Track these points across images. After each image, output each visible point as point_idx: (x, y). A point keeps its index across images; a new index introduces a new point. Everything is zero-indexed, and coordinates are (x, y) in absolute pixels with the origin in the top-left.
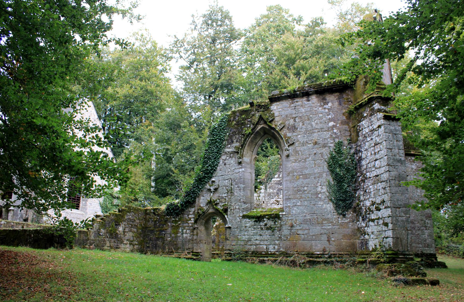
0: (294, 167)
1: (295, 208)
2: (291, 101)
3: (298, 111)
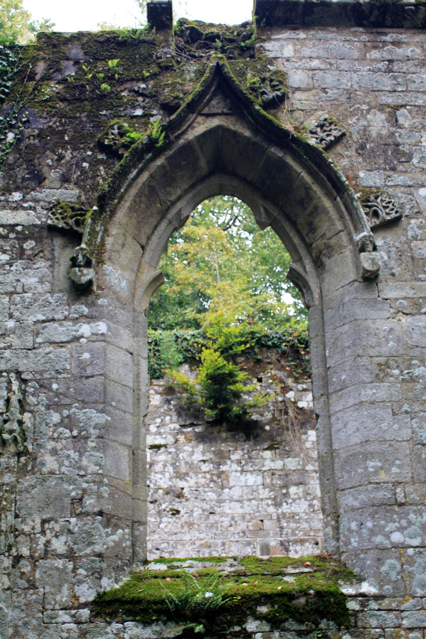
0: (408, 333)
2: (364, 38)
3: (407, 83)
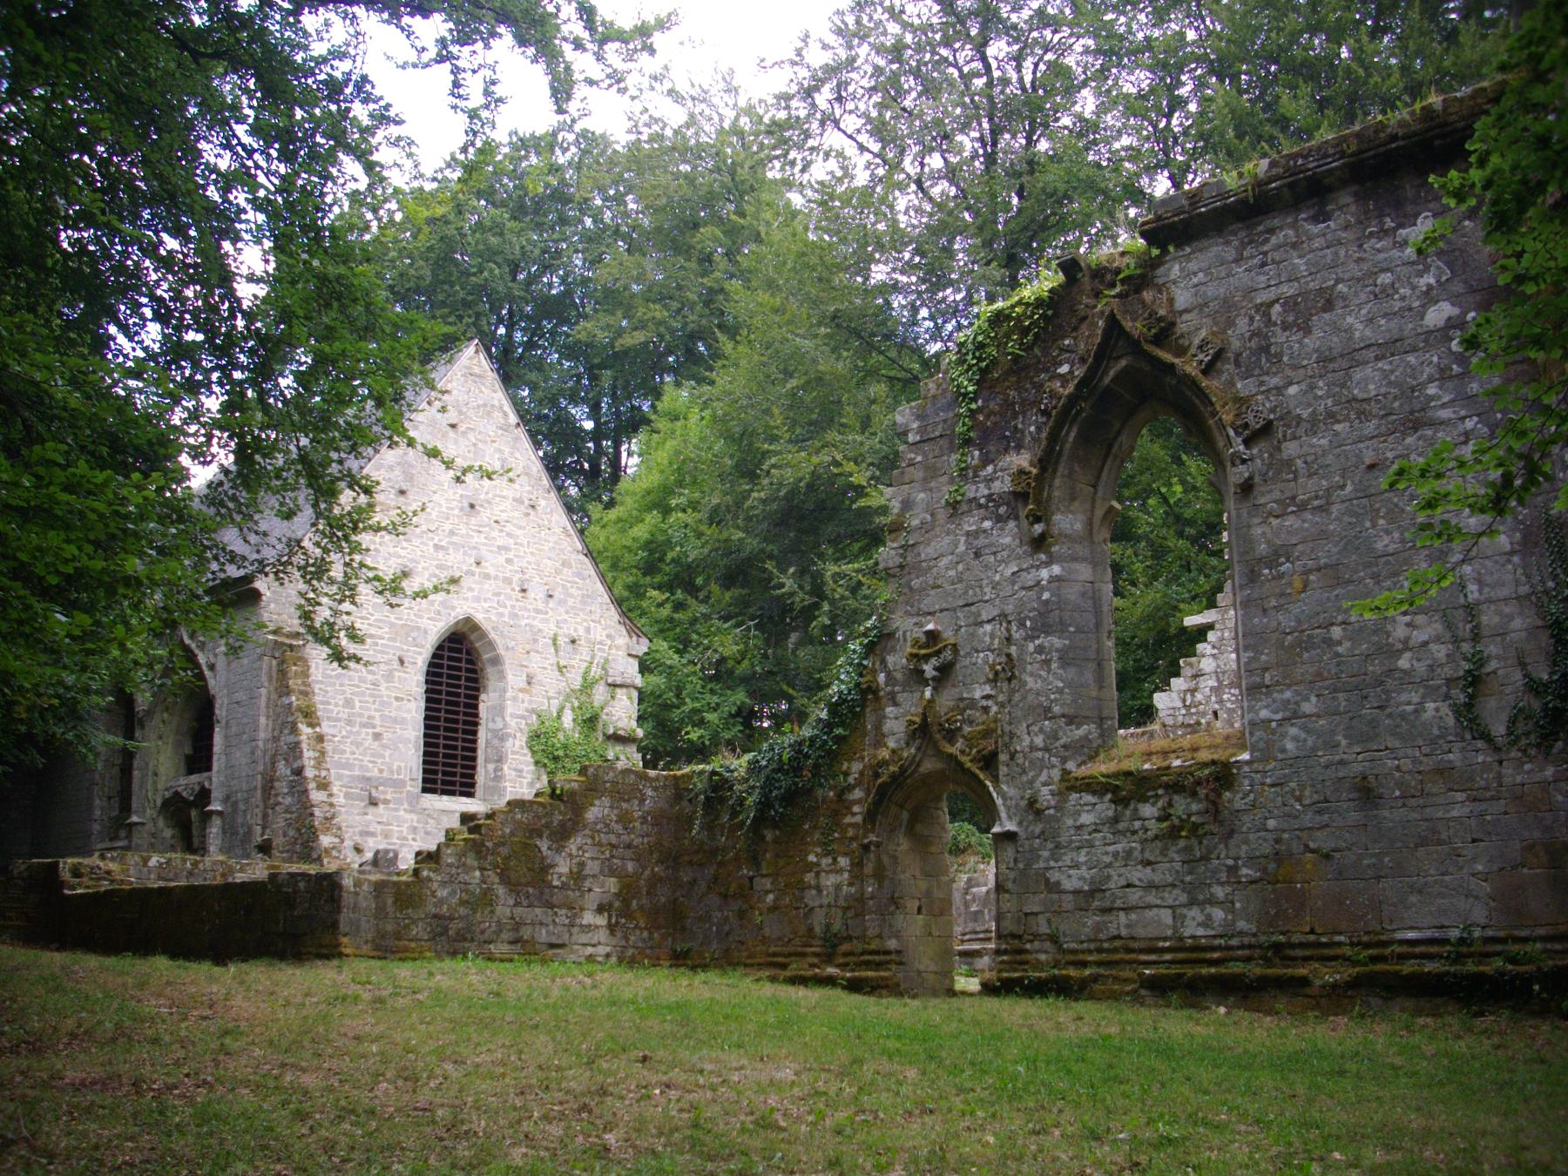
1: (1293, 731)
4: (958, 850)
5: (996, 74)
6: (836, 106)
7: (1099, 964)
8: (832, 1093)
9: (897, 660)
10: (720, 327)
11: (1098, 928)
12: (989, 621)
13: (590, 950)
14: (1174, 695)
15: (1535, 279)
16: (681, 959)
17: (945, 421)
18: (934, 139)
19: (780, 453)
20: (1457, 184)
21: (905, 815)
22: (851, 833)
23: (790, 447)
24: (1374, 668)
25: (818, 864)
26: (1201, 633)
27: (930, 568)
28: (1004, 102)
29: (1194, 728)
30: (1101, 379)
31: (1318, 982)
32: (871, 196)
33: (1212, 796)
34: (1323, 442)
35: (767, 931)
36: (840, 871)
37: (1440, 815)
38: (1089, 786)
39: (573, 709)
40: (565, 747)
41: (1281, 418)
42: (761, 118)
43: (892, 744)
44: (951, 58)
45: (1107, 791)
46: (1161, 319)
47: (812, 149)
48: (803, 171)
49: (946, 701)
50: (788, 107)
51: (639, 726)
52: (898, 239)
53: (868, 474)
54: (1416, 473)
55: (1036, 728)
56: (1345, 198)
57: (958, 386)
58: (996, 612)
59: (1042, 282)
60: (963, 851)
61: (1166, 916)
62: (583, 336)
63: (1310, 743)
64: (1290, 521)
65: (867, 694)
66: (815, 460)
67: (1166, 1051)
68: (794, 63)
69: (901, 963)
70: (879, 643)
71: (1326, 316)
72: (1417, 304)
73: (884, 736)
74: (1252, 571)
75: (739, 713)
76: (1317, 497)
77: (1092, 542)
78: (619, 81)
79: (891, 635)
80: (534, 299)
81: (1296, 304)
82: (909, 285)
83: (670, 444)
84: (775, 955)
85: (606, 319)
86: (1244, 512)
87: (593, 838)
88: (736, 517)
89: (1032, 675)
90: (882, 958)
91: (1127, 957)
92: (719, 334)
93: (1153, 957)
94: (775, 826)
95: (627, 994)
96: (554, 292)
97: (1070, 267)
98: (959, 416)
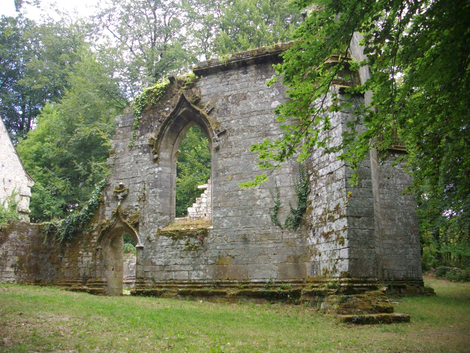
1: (226, 221)
2: (223, 75)
4: (127, 252)
5: (158, 19)
6: (108, 22)
7: (166, 287)
8: (80, 325)
9: (110, 193)
10: (66, 86)
11: (166, 276)
12: (139, 183)
13: (8, 279)
14: (194, 208)
15: (296, 96)
16: (38, 283)
17: (130, 121)
18: (137, 36)
19: (81, 127)
20: (280, 67)
21: (110, 240)
22: (93, 245)
23: (84, 125)
24: (250, 204)
25: (82, 254)
26: (203, 191)
27: (122, 166)
28: (159, 28)
29: (199, 218)
30: (178, 113)
31: (229, 294)
32: (116, 51)
33: (201, 238)
34: (240, 137)
35: (65, 275)
36: (89, 257)
37: (265, 247)
38: (165, 234)
39: (8, 203)
40: (5, 214)
41: (229, 130)
42: (84, 22)
43: (107, 218)
44: (145, 13)
45: (171, 236)
46: (197, 97)
47: (99, 34)
48: (96, 41)
49: (124, 206)
50: (93, 20)
51: (30, 209)
52: (123, 65)
53: (107, 136)
54: (259, 147)
55: (151, 216)
56: (252, 68)
57: (135, 111)
58: (141, 180)
59: (164, 82)
60: (129, 252)
61: (186, 273)
62: (21, 84)
63: (230, 224)
64: (229, 160)
65: (101, 202)
66: (91, 130)
67: (183, 313)
68: (96, 7)
69: (106, 286)
70: (105, 187)
71: (244, 101)
72: (269, 101)
73: (105, 216)
74: (217, 173)
75: (62, 206)
76: (237, 153)
77: (171, 162)
78: (37, 4)
79: (109, 185)
80: (6, 70)
81: (236, 97)
82: (125, 79)
83: (46, 121)
84: (68, 282)
85: (28, 79)
86: (216, 156)
87: (11, 244)
88: (65, 145)
89: (151, 200)
90: (101, 284)
91: (175, 285)
92: (65, 88)
93: (182, 285)
94: (70, 242)
95: (18, 293)
96: (13, 69)
97: (172, 79)
98: (134, 120)
